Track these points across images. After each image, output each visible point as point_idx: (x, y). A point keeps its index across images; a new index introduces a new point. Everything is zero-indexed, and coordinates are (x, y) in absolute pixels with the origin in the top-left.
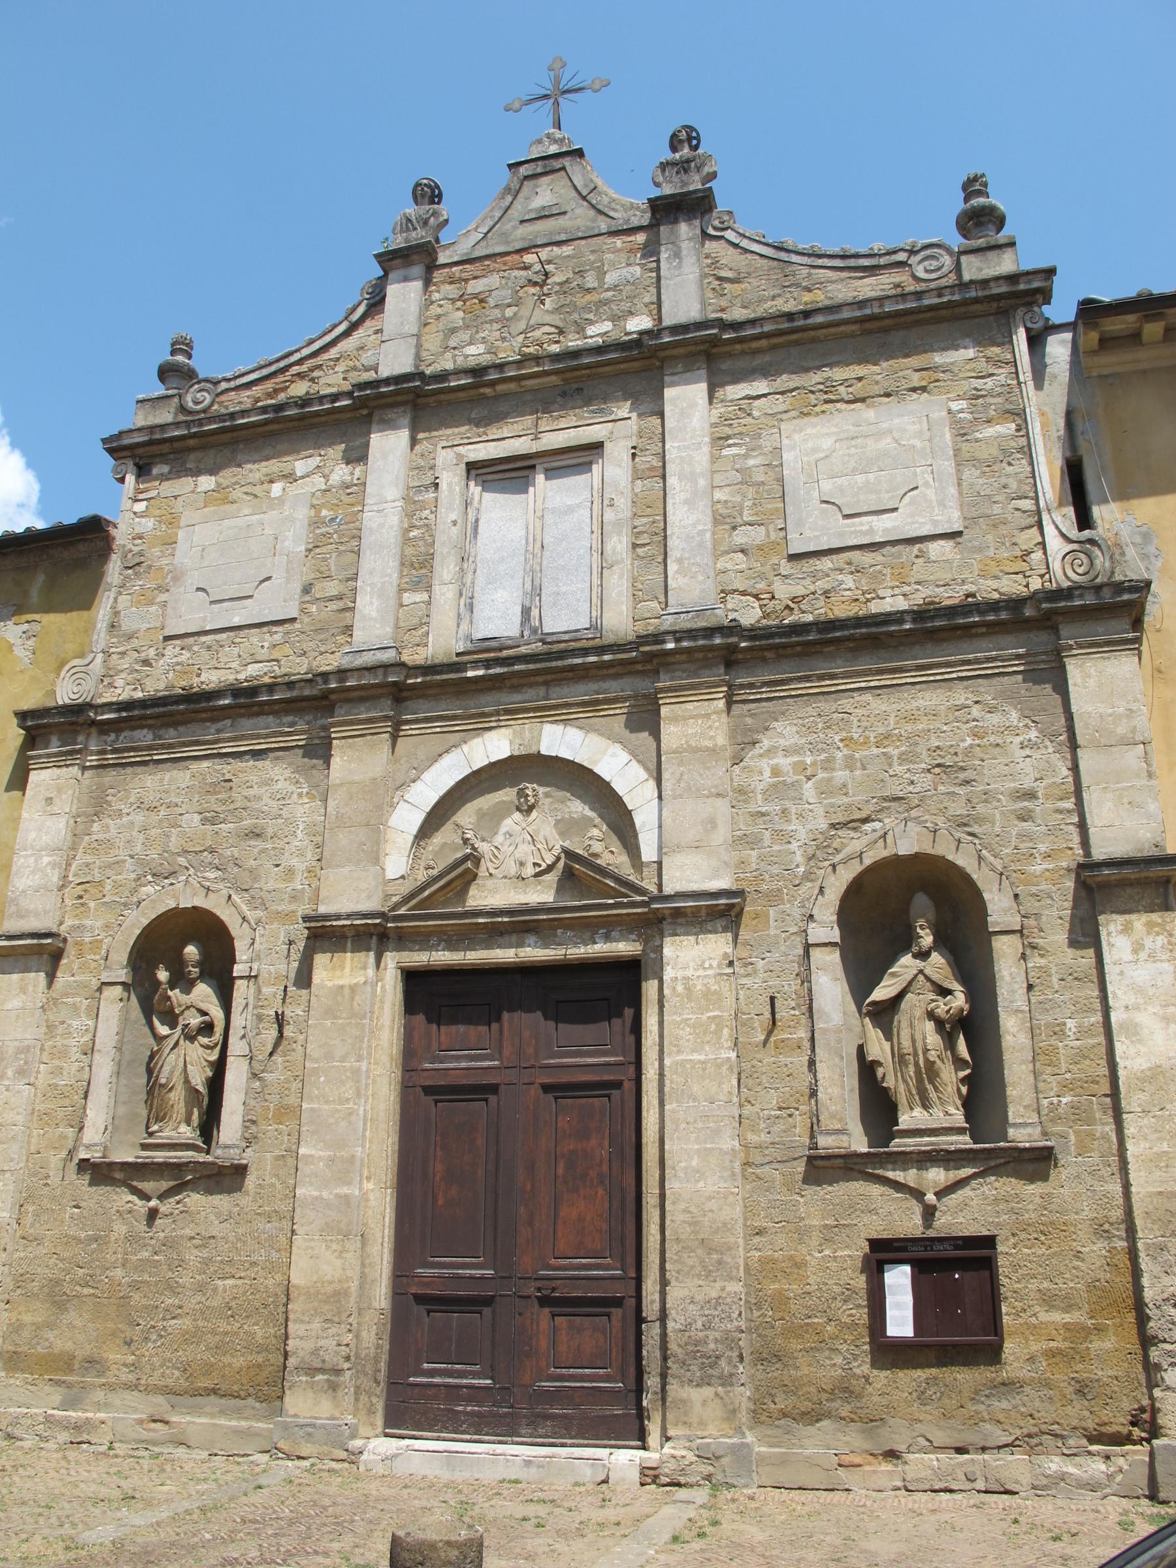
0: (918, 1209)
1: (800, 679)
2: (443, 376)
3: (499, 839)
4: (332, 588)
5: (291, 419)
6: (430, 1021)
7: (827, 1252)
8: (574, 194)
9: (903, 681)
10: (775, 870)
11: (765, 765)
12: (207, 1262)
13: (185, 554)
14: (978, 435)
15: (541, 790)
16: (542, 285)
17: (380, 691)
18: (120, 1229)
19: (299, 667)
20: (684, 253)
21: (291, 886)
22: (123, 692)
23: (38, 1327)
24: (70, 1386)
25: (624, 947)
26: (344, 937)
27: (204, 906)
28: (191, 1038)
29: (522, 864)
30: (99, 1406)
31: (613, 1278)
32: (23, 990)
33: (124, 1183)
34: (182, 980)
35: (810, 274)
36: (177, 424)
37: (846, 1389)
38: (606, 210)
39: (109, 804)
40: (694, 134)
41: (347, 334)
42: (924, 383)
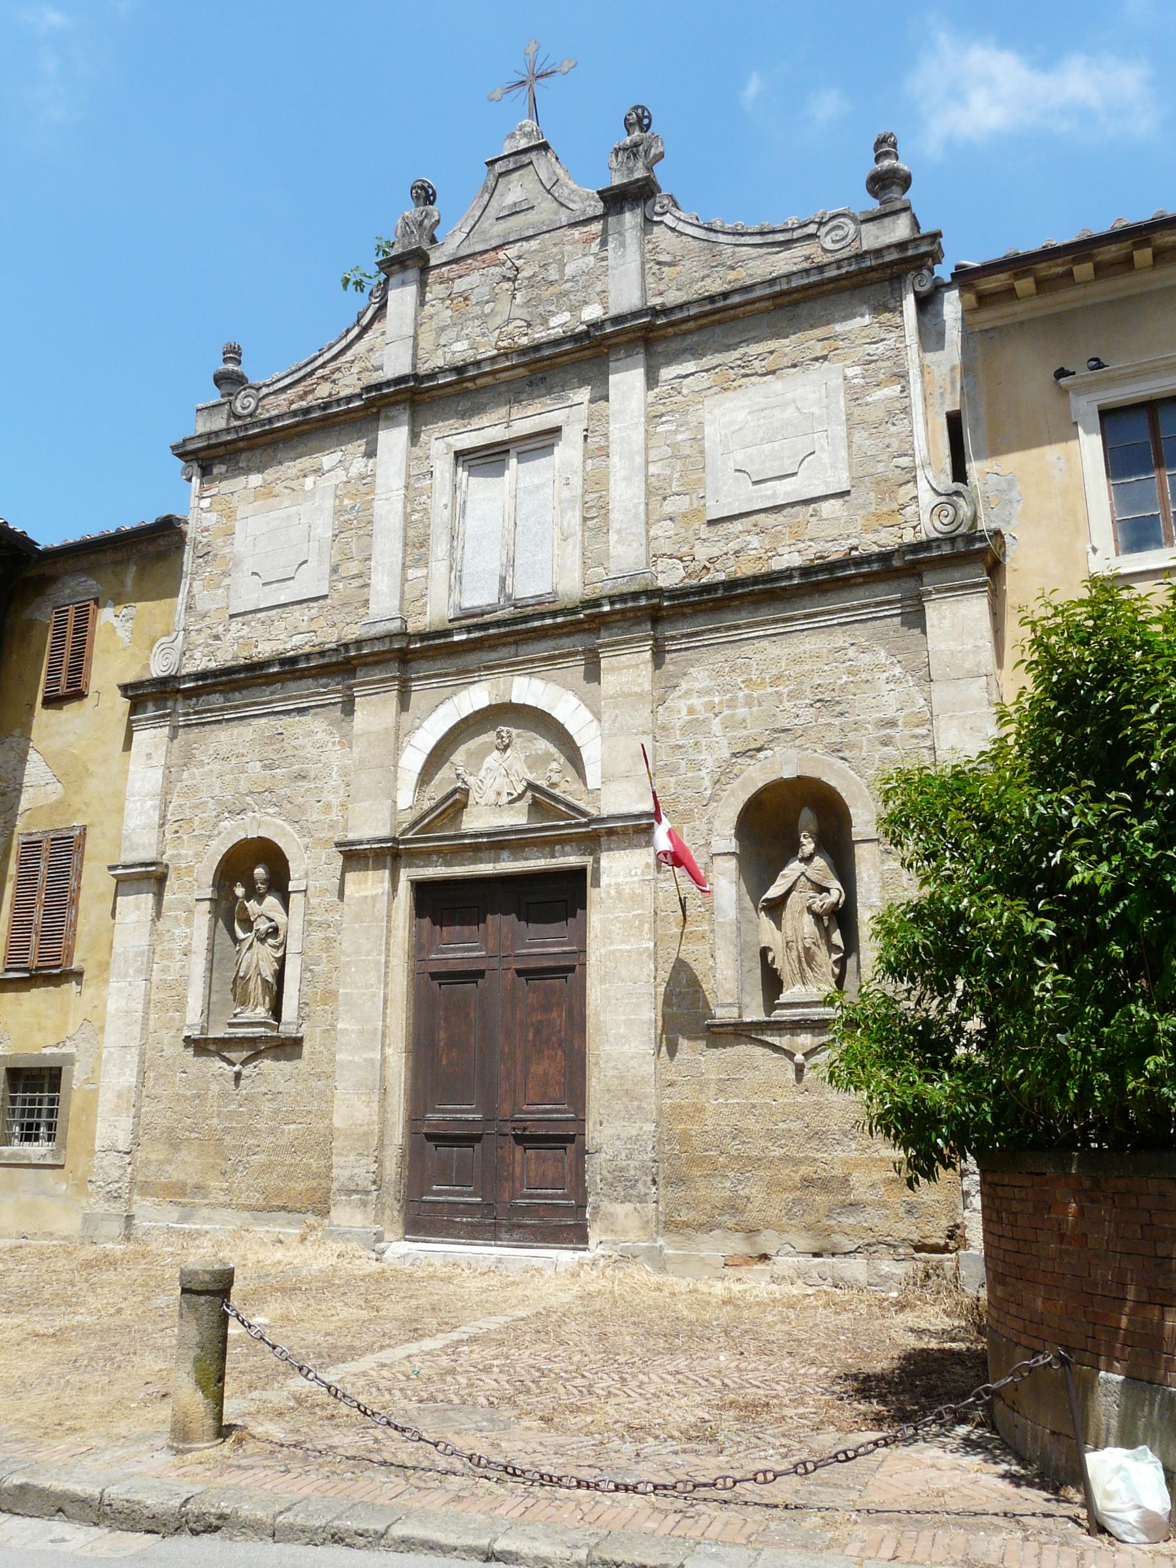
0: (791, 1068)
1: (711, 631)
2: (432, 376)
3: (482, 773)
4: (354, 567)
5: (317, 420)
6: (434, 924)
7: (721, 1100)
8: (541, 188)
9: (794, 628)
10: (688, 793)
11: (683, 705)
12: (276, 1112)
13: (241, 544)
14: (869, 399)
15: (514, 732)
16: (514, 280)
17: (389, 656)
18: (215, 1088)
19: (330, 637)
20: (628, 241)
21: (329, 817)
22: (199, 662)
23: (161, 1163)
24: (184, 1205)
25: (572, 860)
26: (366, 857)
27: (266, 836)
28: (262, 940)
29: (499, 794)
30: (209, 1220)
31: (567, 1120)
32: (137, 907)
33: (218, 1054)
34: (253, 893)
35: (734, 253)
36: (228, 430)
37: (733, 1207)
38: (566, 202)
39: (194, 756)
40: (646, 114)
41: (359, 337)
42: (825, 353)
